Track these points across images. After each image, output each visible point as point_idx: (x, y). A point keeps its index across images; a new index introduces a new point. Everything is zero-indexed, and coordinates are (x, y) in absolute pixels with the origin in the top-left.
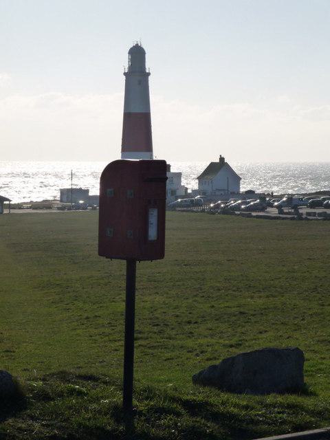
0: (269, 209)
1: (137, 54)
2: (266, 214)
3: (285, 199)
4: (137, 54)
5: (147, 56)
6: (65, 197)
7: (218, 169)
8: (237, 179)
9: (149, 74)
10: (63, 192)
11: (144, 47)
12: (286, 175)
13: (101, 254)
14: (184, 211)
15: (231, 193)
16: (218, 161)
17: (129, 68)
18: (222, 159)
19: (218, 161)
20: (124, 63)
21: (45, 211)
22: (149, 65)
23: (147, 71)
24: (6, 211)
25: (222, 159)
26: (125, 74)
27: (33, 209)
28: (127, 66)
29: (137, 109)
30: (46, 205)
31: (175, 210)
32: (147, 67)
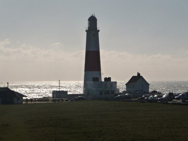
0: (173, 100)
1: (93, 21)
2: (172, 102)
3: (181, 95)
4: (93, 21)
5: (98, 22)
6: (55, 95)
7: (137, 81)
8: (148, 85)
9: (99, 31)
10: (54, 93)
11: (96, 17)
12: (169, 85)
13: (99, 78)
14: (124, 101)
15: (144, 92)
16: (137, 75)
17: (89, 28)
18: (139, 74)
19: (137, 75)
20: (86, 25)
21: (45, 102)
22: (99, 26)
23: (98, 29)
24: (24, 103)
25: (139, 74)
26: (86, 31)
27: (39, 101)
28: (87, 27)
29: (92, 49)
30: (45, 99)
31: (119, 100)
32: (98, 27)
